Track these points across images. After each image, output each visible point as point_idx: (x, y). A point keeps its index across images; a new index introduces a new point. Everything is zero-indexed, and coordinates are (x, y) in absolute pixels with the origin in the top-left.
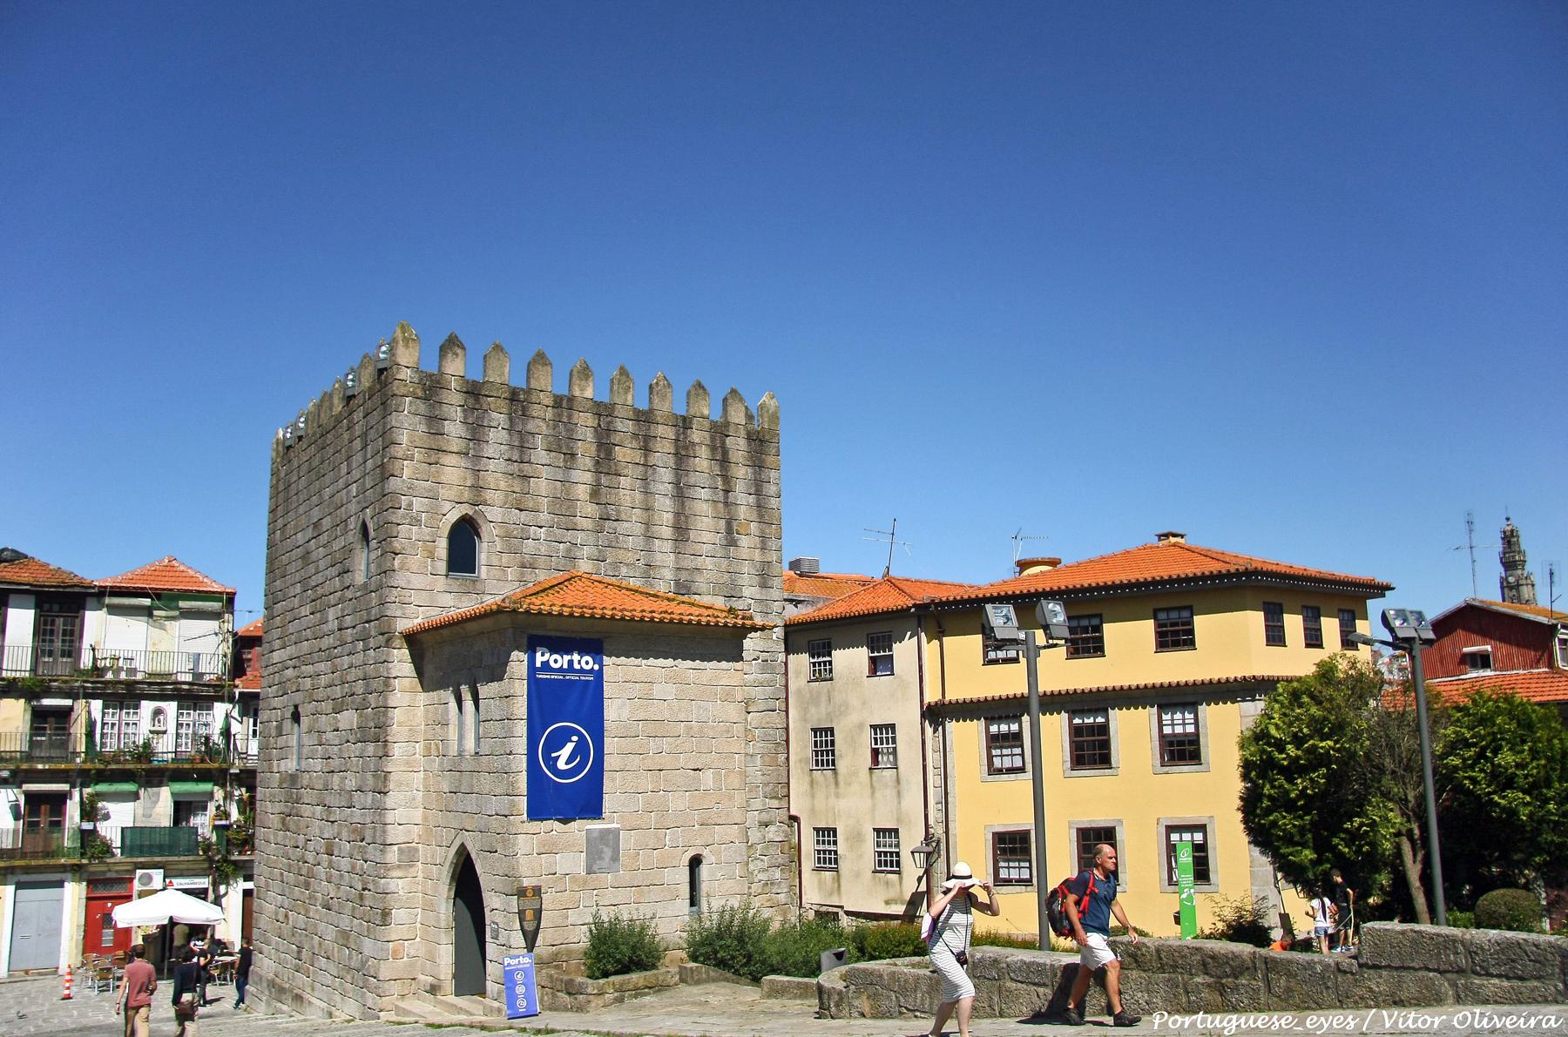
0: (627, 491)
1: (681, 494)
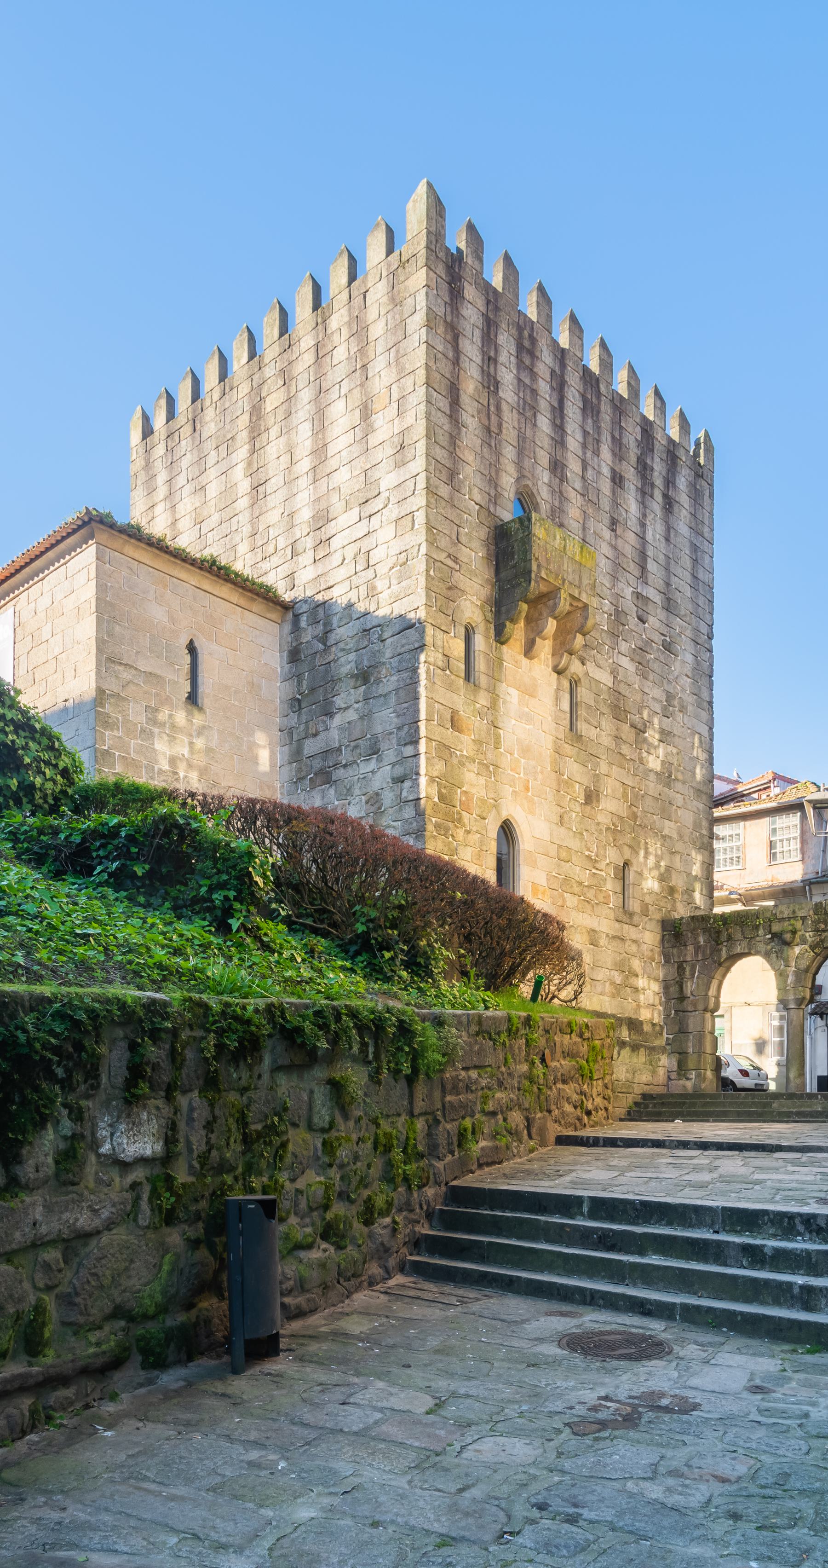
0: (274, 448)
1: (559, 427)
